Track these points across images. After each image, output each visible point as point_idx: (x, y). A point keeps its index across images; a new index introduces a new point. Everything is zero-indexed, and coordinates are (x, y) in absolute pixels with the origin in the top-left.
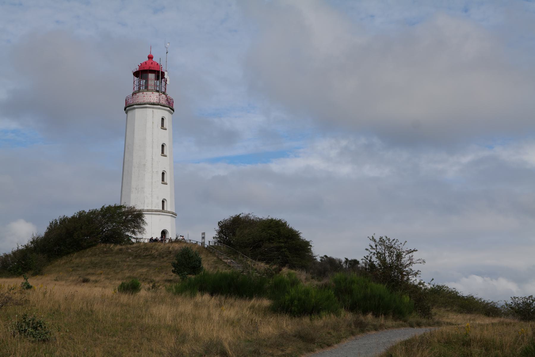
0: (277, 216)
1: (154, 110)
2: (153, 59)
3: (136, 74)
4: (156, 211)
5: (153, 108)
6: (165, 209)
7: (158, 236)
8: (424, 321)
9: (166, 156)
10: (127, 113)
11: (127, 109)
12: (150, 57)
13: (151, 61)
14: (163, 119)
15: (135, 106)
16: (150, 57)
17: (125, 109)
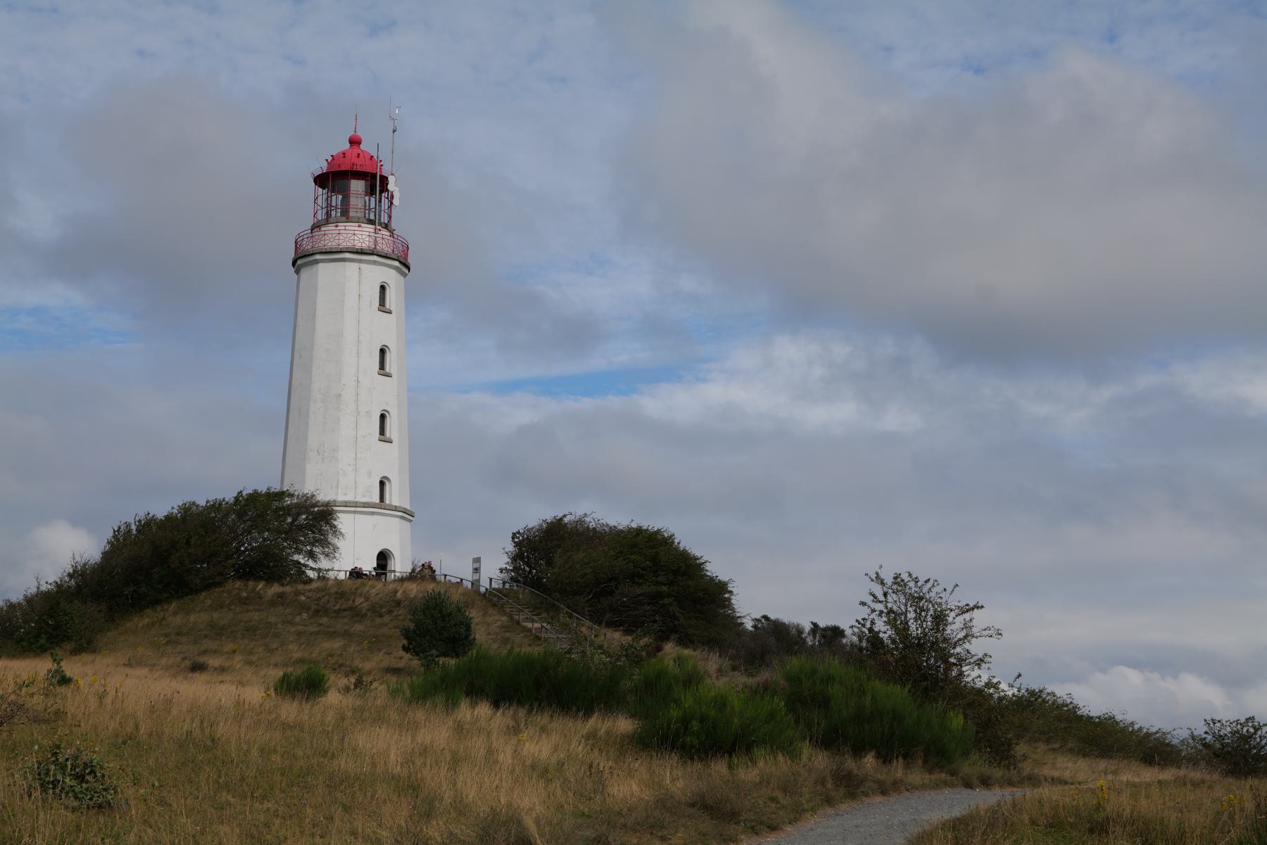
0: (650, 522)
1: (363, 266)
3: (321, 180)
4: (366, 505)
5: (360, 261)
8: (998, 773)
9: (389, 375)
10: (297, 272)
11: (299, 262)
12: (355, 142)
13: (356, 151)
14: (383, 288)
15: (318, 257)
16: (355, 142)
17: (294, 264)
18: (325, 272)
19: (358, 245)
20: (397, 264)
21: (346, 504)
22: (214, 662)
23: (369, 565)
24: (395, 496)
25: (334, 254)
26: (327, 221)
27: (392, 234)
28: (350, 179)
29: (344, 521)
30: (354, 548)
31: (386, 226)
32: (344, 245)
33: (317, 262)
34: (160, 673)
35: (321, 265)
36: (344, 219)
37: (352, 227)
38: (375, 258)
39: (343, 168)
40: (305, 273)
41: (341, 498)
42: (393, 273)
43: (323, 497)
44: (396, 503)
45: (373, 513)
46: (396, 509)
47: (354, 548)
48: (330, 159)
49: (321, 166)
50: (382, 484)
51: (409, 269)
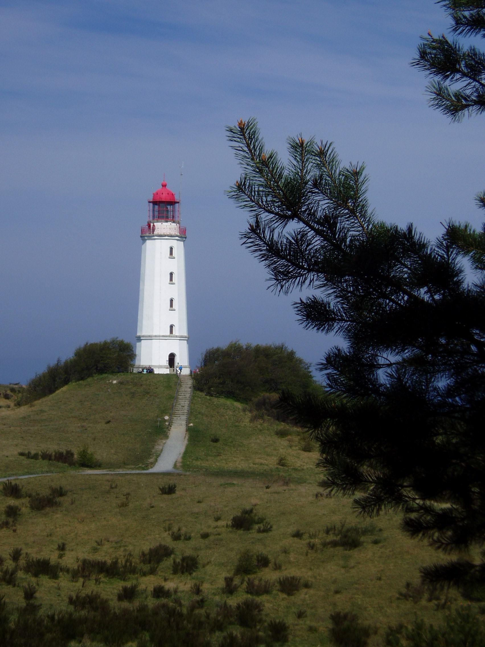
3: (149, 202)
4: (163, 336)
5: (161, 239)
7: (165, 361)
12: (164, 186)
14: (171, 249)
16: (164, 186)
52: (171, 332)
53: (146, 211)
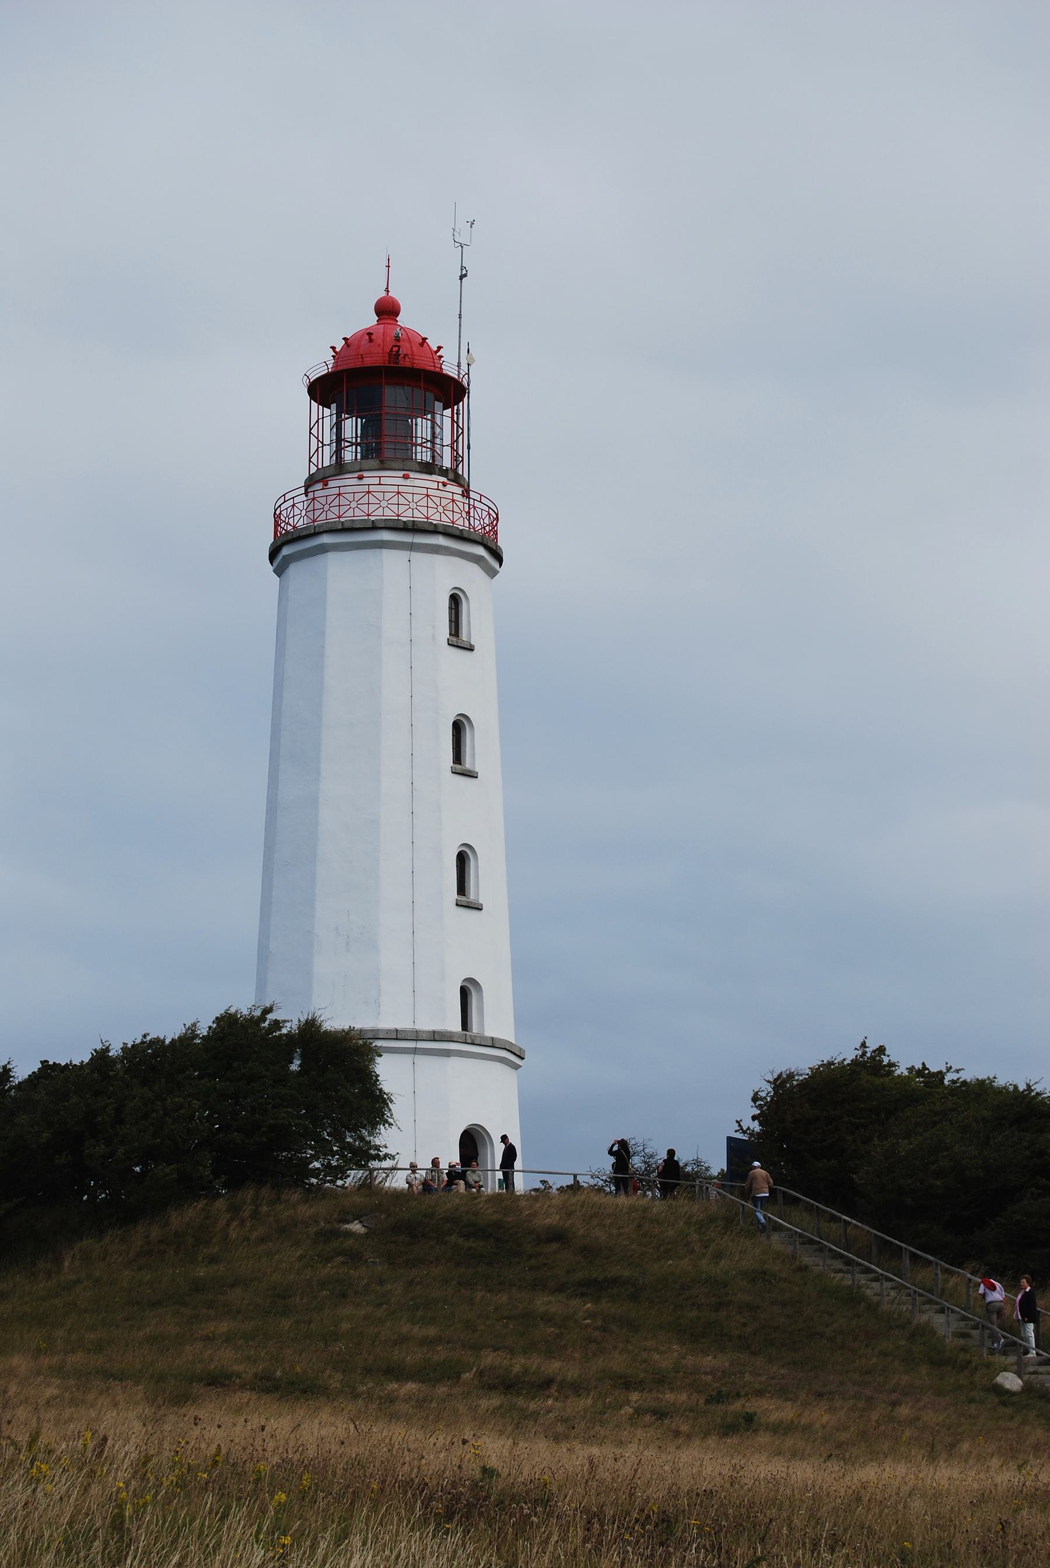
2: (402, 320)
5: (412, 547)
6: (475, 1028)
9: (471, 775)
10: (279, 572)
11: (286, 551)
12: (387, 310)
15: (326, 539)
16: (387, 310)
17: (273, 555)
18: (340, 572)
19: (407, 516)
20: (481, 551)
21: (397, 1035)
22: (774, 1410)
23: (451, 1156)
24: (496, 1019)
25: (359, 532)
26: (340, 468)
27: (466, 493)
28: (385, 390)
29: (390, 1072)
30: (421, 1125)
31: (457, 479)
32: (378, 514)
33: (323, 549)
34: (247, 1395)
35: (332, 557)
36: (374, 463)
37: (392, 478)
38: (441, 541)
39: (369, 362)
40: (294, 570)
41: (387, 1022)
42: (475, 569)
43: (334, 1021)
44: (491, 1031)
45: (447, 1053)
46: (493, 1043)
47: (421, 1125)
48: (340, 345)
49: (321, 363)
50: (464, 993)
51: (499, 559)
52: (465, 1024)
53: (287, 435)
